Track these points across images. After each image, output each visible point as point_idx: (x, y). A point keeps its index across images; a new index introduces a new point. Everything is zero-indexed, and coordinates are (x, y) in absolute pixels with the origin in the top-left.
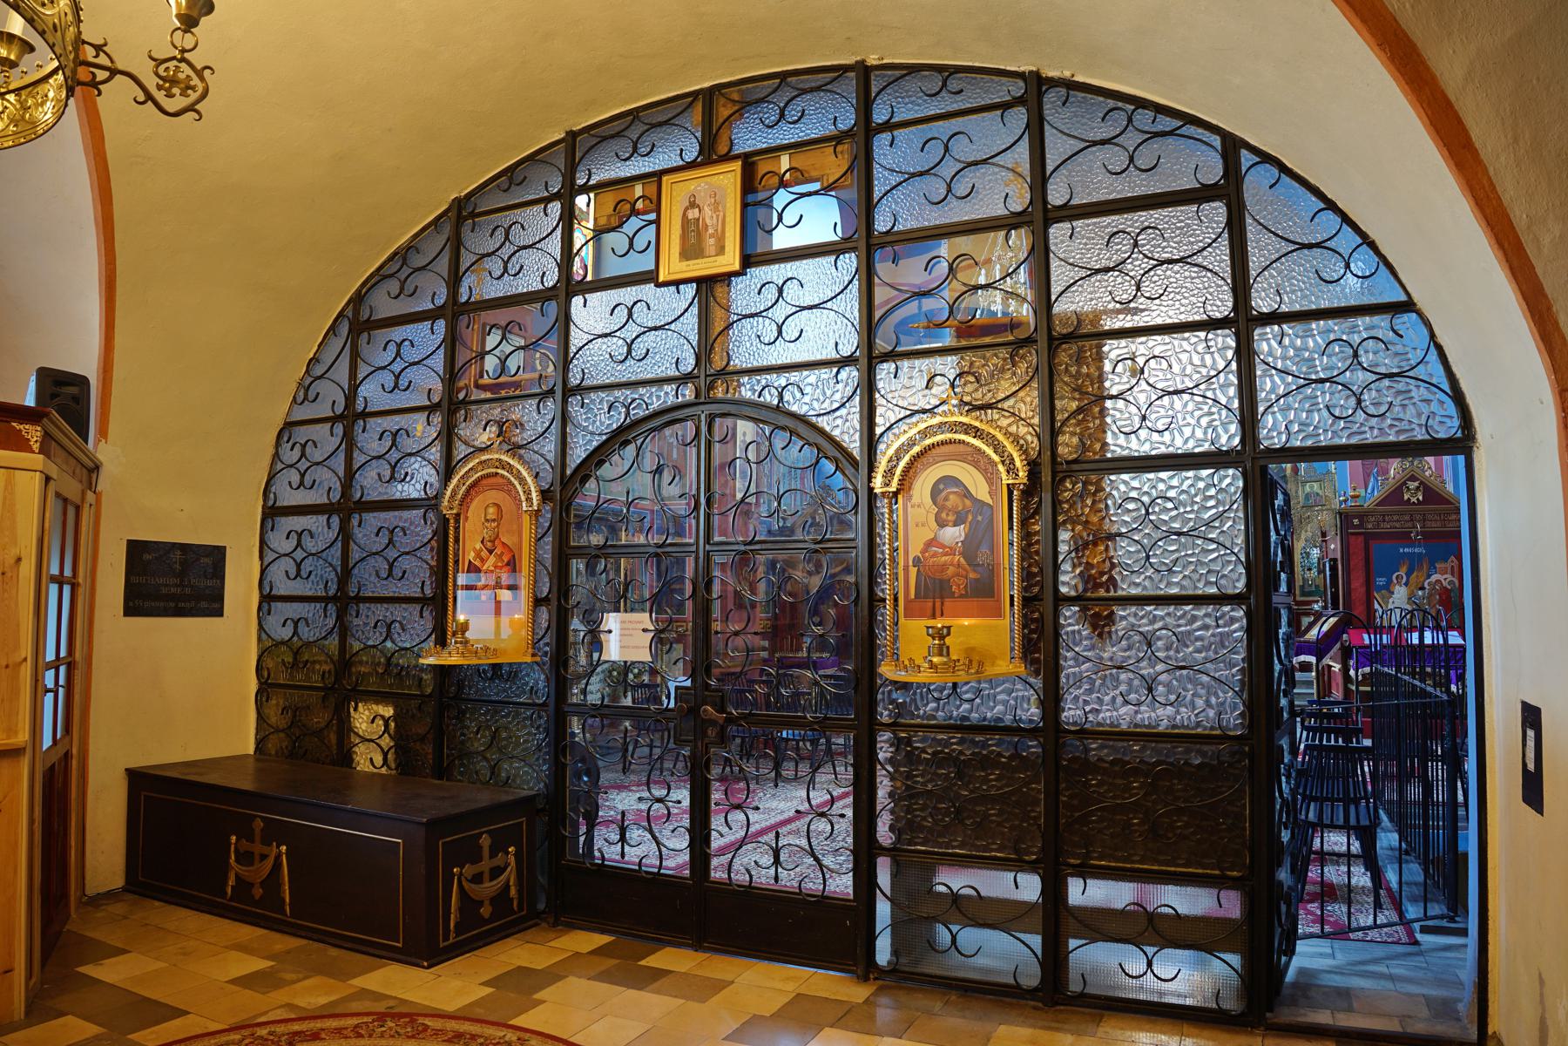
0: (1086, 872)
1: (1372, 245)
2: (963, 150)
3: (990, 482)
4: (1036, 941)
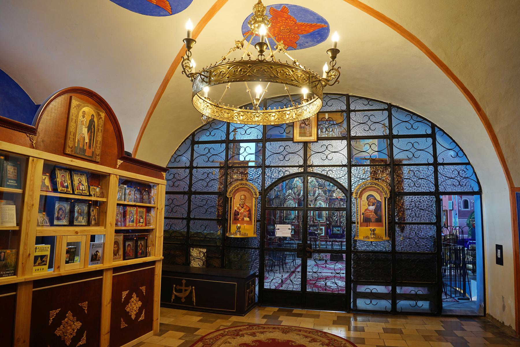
0: (402, 285)
1: (462, 151)
2: (373, 119)
3: (381, 196)
4: (390, 301)
